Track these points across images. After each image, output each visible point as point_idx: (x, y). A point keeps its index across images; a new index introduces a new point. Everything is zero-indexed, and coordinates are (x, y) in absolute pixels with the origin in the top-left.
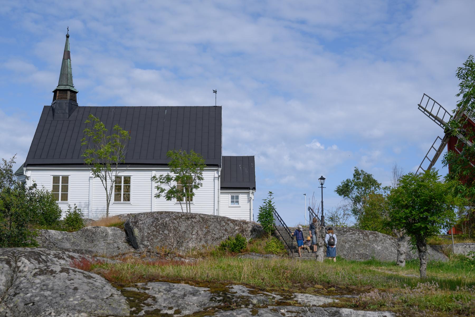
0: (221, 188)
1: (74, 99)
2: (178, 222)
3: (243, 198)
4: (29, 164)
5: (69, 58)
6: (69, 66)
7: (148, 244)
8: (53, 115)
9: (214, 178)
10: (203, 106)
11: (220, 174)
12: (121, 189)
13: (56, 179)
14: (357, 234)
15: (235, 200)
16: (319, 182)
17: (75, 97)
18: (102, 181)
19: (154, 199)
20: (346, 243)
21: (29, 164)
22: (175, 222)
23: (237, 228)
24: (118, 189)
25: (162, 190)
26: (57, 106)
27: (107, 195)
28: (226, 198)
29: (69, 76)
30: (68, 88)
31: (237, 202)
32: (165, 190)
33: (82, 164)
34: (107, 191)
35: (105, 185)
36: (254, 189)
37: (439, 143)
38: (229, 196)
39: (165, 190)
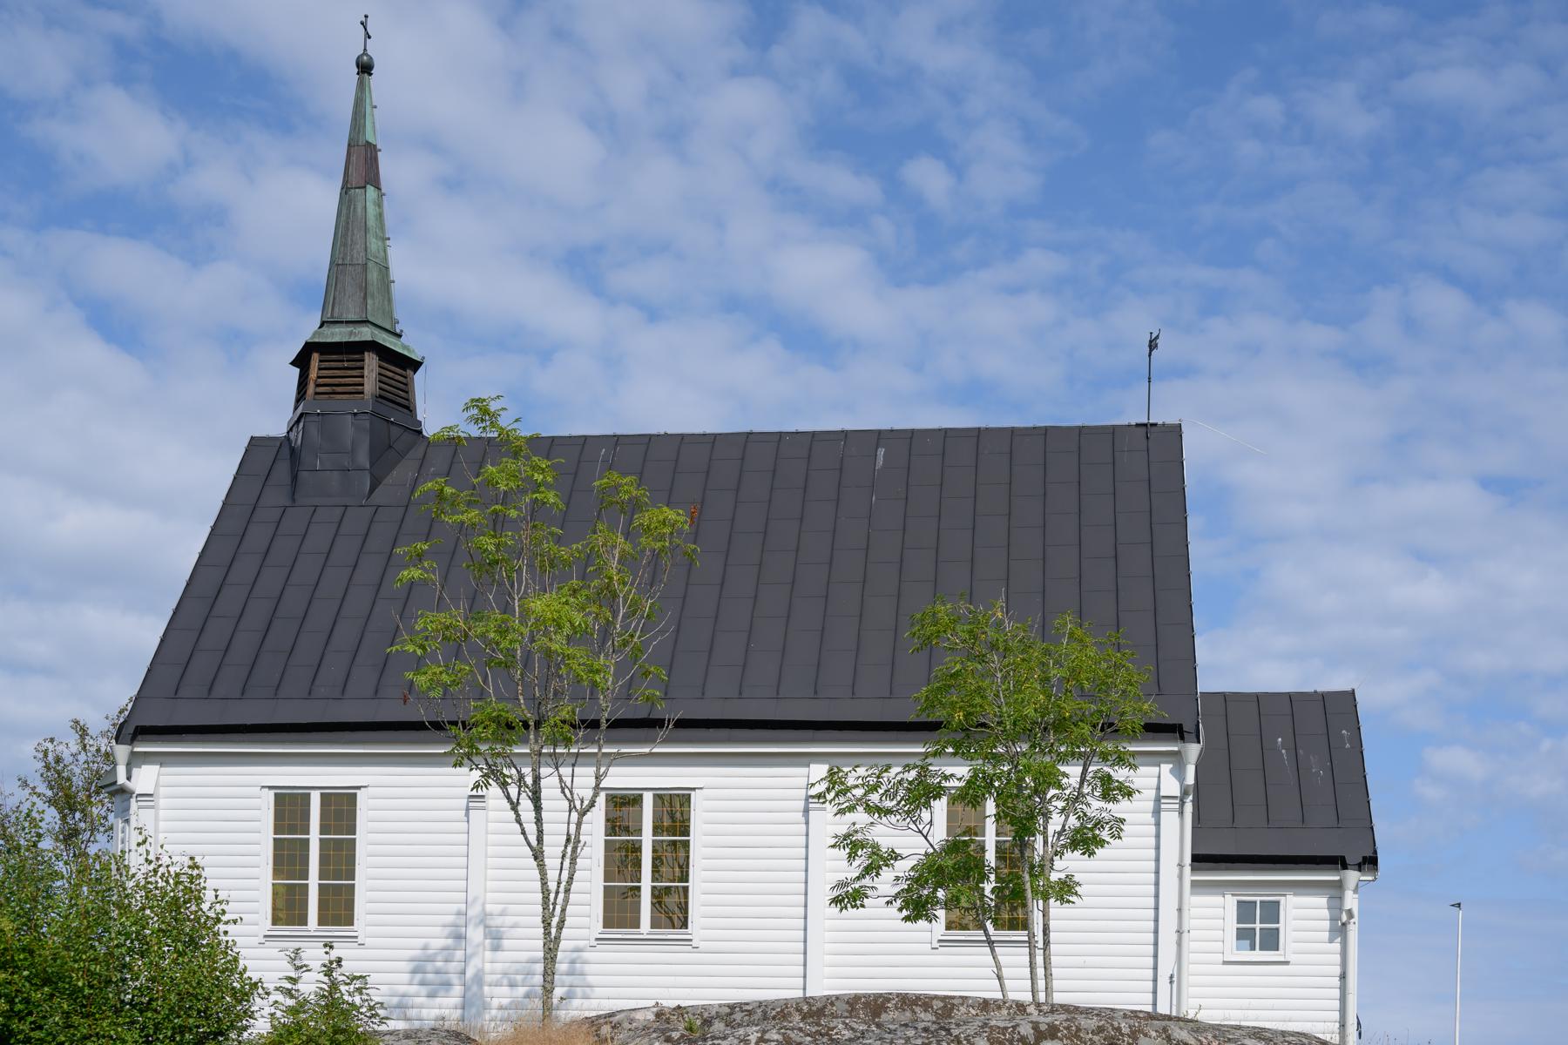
0: (1196, 858)
1: (398, 398)
3: (1303, 912)
4: (154, 724)
5: (372, 178)
6: (372, 222)
8: (295, 478)
9: (1158, 799)
10: (1080, 424)
11: (1190, 779)
12: (638, 864)
13: (290, 807)
15: (1258, 929)
17: (406, 389)
18: (514, 806)
19: (823, 912)
21: (154, 724)
24: (622, 859)
25: (879, 860)
26: (313, 430)
27: (545, 891)
28: (1214, 912)
29: (373, 275)
30: (365, 334)
31: (1271, 941)
32: (894, 856)
33: (417, 726)
34: (542, 867)
35: (531, 828)
36: (1370, 862)
38: (1230, 902)
39: (894, 856)
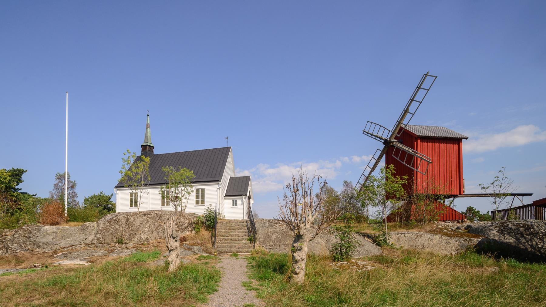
7: (100, 236)
15: (235, 204)
20: (273, 234)
22: (132, 218)
23: (187, 221)
28: (229, 202)
31: (236, 204)
37: (379, 153)
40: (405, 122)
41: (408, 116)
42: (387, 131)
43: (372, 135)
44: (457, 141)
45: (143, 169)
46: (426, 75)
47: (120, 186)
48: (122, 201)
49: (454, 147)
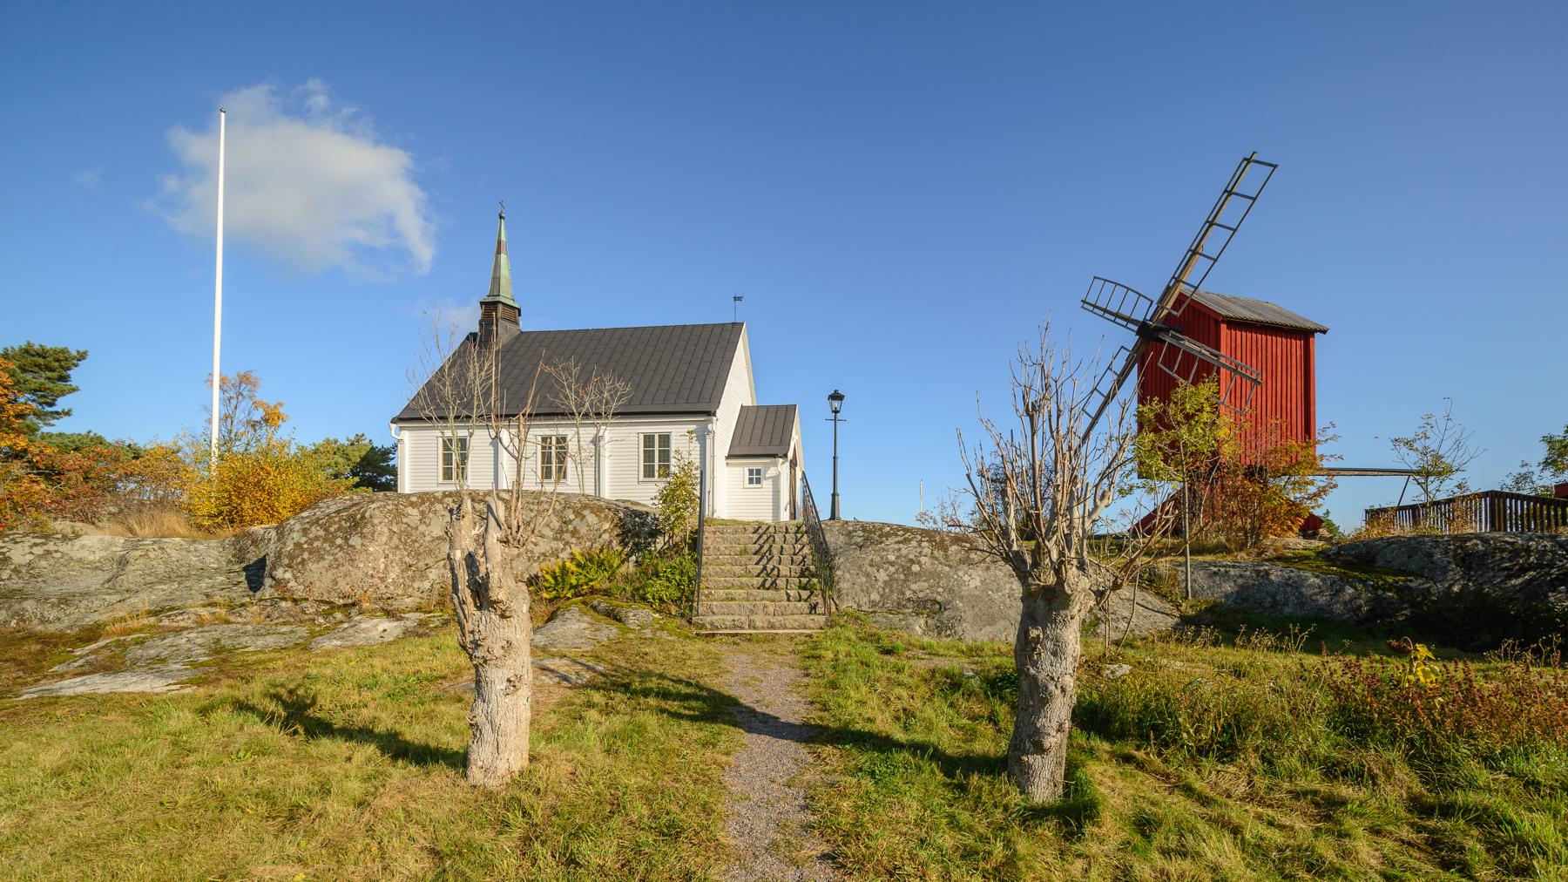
2: (422, 513)
14: (914, 543)
15: (755, 478)
16: (826, 407)
22: (414, 512)
40: (1192, 277)
41: (1200, 265)
42: (1144, 304)
43: (1105, 311)
44: (1304, 335)
45: (484, 371)
46: (1249, 161)
47: (407, 418)
48: (417, 460)
49: (1297, 344)
